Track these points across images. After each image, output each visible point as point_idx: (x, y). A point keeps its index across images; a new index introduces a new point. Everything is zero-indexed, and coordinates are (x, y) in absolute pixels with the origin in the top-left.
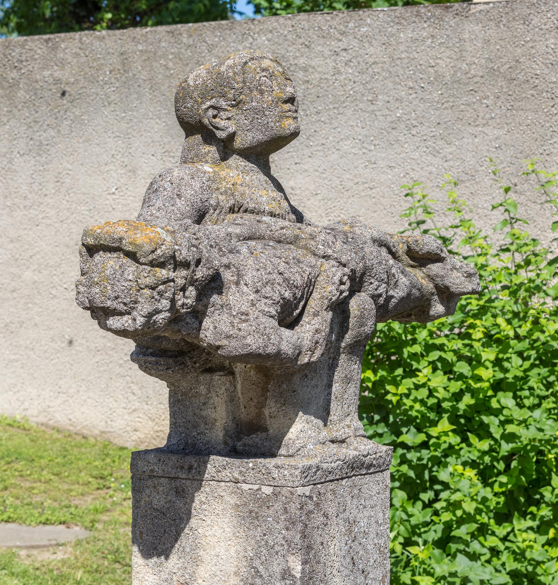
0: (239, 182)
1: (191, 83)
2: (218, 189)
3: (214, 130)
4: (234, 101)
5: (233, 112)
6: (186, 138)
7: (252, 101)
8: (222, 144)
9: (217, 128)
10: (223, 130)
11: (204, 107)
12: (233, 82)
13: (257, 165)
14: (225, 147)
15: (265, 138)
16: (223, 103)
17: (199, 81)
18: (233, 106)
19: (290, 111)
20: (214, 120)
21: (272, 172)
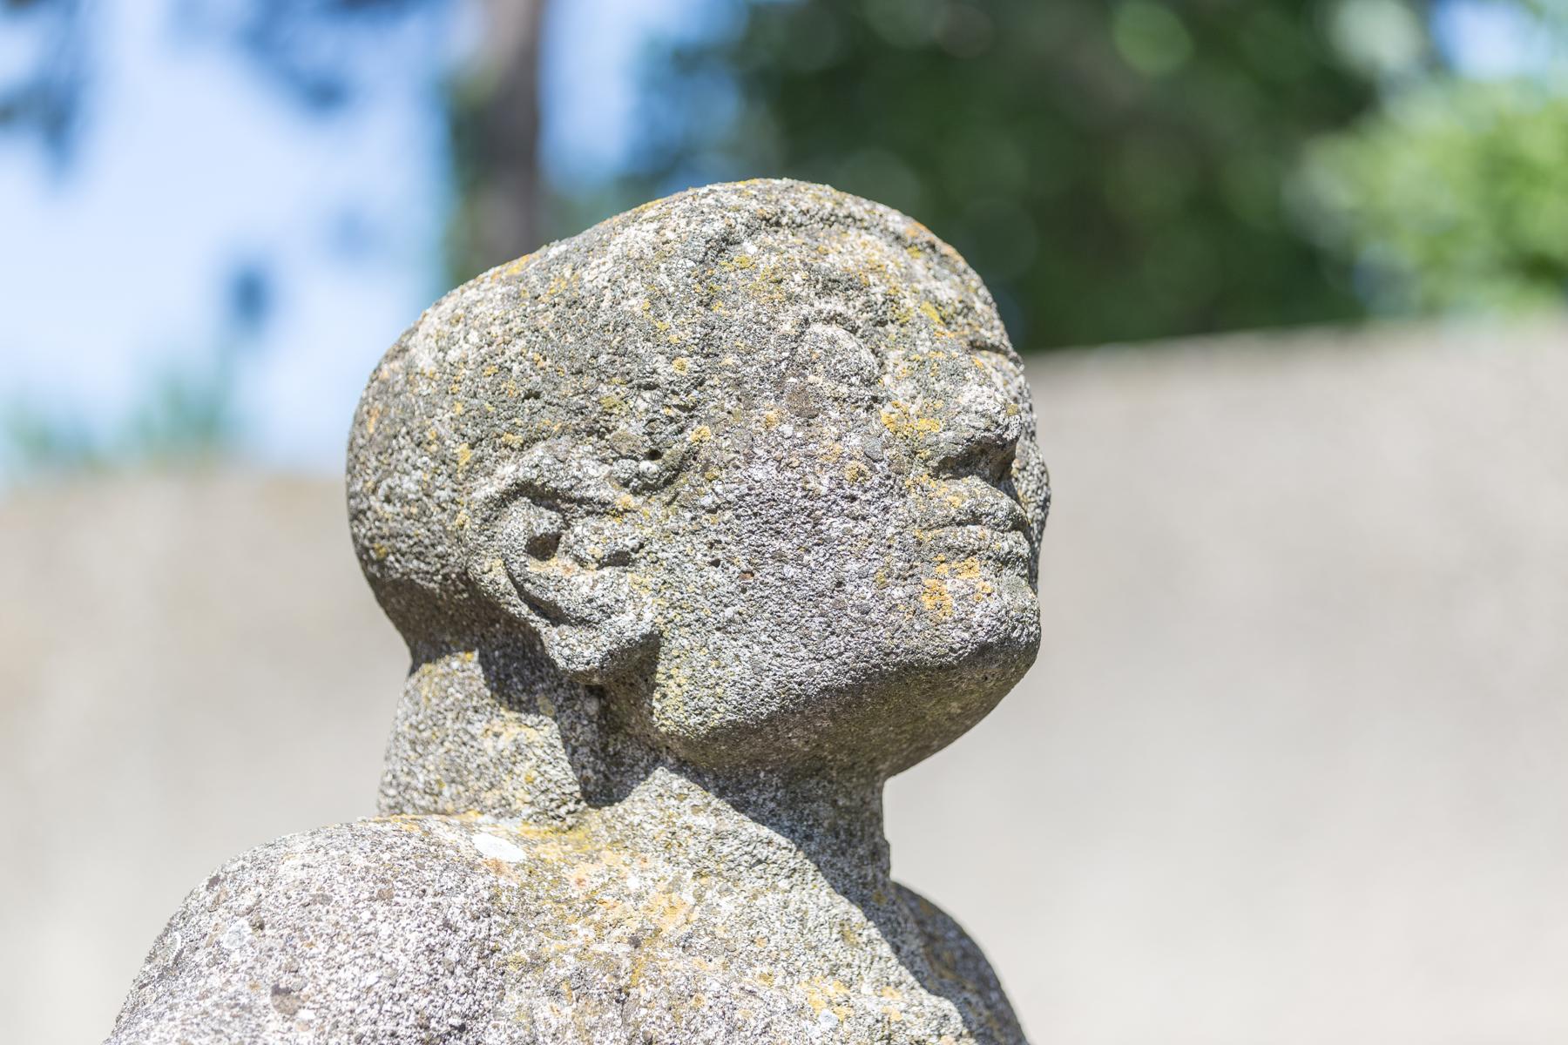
0: (672, 926)
2: (537, 963)
3: (539, 623)
4: (654, 455)
5: (651, 518)
7: (750, 459)
8: (592, 707)
9: (555, 615)
10: (583, 622)
11: (487, 488)
12: (643, 348)
13: (791, 832)
14: (609, 723)
15: (826, 674)
16: (590, 472)
17: (467, 348)
18: (647, 488)
19: (976, 519)
20: (534, 567)
21: (903, 870)
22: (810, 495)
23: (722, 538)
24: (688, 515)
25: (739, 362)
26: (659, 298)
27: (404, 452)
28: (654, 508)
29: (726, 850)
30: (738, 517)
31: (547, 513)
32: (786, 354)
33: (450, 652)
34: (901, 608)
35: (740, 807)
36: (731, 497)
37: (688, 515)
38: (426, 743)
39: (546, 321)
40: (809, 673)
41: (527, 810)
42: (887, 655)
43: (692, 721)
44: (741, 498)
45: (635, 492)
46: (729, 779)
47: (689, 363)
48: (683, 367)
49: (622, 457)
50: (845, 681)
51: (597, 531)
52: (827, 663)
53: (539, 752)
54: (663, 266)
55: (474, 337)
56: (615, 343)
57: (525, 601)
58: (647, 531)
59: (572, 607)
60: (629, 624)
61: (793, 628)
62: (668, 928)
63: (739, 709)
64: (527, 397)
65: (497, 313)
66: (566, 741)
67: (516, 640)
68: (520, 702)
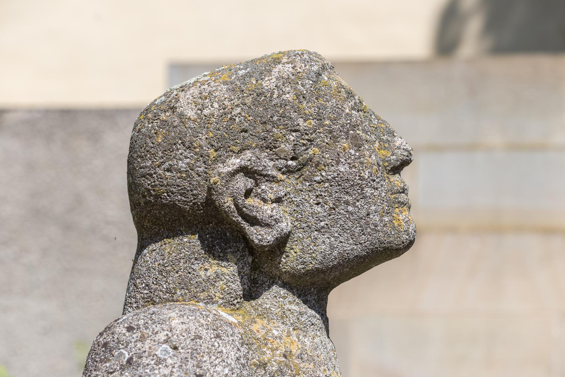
0: (295, 351)
1: (191, 113)
3: (245, 225)
5: (287, 186)
6: (141, 247)
7: (338, 163)
9: (254, 221)
10: (268, 225)
11: (225, 169)
16: (269, 165)
18: (289, 171)
22: (362, 178)
23: (323, 194)
24: (308, 184)
25: (331, 123)
26: (299, 95)
27: (180, 151)
28: (292, 180)
29: (303, 319)
30: (331, 186)
31: (250, 180)
32: (349, 121)
33: (182, 234)
34: (388, 225)
35: (305, 302)
36: (329, 177)
37: (308, 184)
38: (168, 272)
39: (249, 101)
40: (352, 250)
41: (221, 301)
42: (381, 243)
43: (299, 267)
44: (334, 178)
45: (283, 173)
46: (302, 291)
47: (313, 122)
48: (310, 124)
49: (281, 158)
50: (364, 253)
51: (271, 188)
52: (359, 246)
53: (227, 277)
54: (300, 82)
55: (216, 105)
56: (281, 112)
57: (240, 215)
58: (289, 189)
59: (264, 219)
60: (285, 226)
61: (349, 231)
62: (294, 351)
63: (321, 263)
64: (242, 132)
65: (226, 96)
66: (239, 273)
67: (218, 231)
68: (219, 256)
